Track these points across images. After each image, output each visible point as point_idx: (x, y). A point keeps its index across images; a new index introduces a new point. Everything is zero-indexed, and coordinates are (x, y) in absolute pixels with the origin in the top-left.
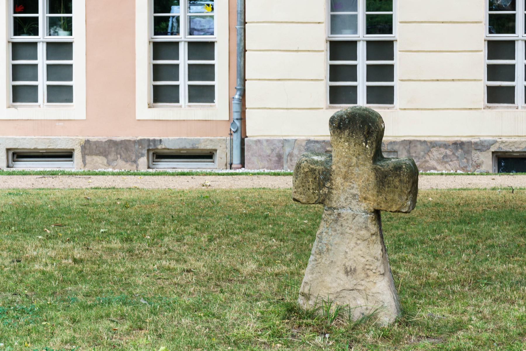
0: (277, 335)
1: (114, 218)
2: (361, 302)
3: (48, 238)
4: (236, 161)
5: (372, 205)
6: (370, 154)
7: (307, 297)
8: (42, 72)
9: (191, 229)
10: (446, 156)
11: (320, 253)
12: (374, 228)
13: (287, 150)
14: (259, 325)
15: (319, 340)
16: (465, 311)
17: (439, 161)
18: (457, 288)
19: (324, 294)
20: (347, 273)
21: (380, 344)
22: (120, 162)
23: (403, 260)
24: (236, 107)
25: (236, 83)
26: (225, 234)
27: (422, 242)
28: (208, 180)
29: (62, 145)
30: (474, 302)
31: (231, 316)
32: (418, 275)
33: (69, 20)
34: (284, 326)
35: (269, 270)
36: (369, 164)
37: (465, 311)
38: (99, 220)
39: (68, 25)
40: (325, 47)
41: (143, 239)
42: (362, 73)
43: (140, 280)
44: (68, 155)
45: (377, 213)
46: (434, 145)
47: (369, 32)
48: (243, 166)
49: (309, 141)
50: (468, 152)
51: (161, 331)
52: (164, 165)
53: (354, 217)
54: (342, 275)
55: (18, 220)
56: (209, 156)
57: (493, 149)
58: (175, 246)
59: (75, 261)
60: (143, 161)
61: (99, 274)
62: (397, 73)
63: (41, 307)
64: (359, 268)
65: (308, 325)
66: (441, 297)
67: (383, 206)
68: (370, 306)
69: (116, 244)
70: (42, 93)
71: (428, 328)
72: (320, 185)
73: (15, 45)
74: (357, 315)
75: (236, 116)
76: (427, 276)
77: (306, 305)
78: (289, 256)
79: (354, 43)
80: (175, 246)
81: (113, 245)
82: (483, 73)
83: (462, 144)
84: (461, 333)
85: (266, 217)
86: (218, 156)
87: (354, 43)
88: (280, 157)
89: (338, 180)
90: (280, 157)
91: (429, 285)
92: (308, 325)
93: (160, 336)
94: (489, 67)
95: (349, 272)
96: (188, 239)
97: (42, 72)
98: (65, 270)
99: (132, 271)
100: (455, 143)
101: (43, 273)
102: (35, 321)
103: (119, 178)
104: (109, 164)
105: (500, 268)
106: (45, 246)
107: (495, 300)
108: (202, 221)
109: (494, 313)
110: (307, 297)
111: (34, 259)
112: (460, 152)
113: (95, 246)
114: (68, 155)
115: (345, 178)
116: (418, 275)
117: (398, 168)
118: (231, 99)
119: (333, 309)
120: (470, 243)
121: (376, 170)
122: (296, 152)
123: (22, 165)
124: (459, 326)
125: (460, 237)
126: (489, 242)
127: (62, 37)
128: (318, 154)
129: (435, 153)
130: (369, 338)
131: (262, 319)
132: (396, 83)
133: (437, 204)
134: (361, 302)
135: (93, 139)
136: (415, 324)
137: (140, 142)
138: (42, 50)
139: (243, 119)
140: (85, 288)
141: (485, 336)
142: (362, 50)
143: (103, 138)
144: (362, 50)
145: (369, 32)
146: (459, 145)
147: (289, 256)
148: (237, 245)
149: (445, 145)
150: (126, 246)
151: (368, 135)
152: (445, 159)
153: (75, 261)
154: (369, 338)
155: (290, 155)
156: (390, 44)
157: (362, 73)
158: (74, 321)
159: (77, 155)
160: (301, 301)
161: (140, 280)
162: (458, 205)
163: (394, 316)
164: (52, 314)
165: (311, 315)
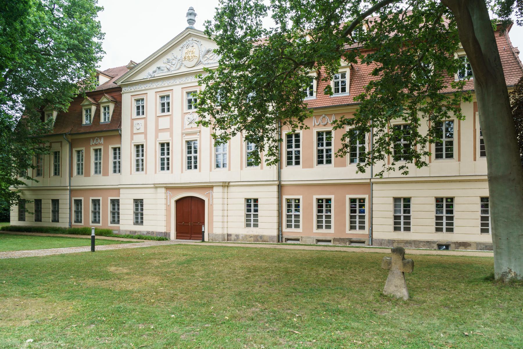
0: (378, 301)
1: (340, 262)
2: (399, 294)
3: (324, 267)
4: (370, 244)
5: (402, 271)
6: (401, 258)
7: (385, 291)
8: (324, 222)
9: (358, 266)
10: (424, 245)
11: (389, 281)
12: (402, 276)
13: (383, 242)
14: (373, 298)
15: (388, 303)
16: (426, 297)
17: (422, 246)
18: (425, 289)
19: (389, 291)
20: (395, 287)
21: (404, 305)
22: (342, 243)
23: (411, 279)
24: (370, 231)
25: (370, 225)
26: (366, 268)
27: (416, 273)
28: (363, 249)
29: (328, 239)
30: (429, 294)
31: (366, 294)
32: (415, 284)
33: (330, 210)
34: (379, 299)
35: (377, 281)
36: (401, 261)
37: (426, 297)
38: (336, 262)
39: (330, 211)
40: (393, 217)
41: (346, 269)
42: (402, 223)
43: (345, 282)
44: (330, 241)
45: (403, 273)
46: (421, 242)
47: (404, 213)
48: (372, 245)
49: (389, 240)
50: (430, 244)
51: (349, 298)
52: (353, 245)
53: (397, 273)
54: (394, 287)
55: (318, 261)
56: (364, 242)
57: (437, 243)
58: (354, 271)
59: (330, 275)
60: (348, 243)
61: (335, 279)
62: (454, 224)
63: (322, 289)
64: (399, 286)
65: (385, 299)
66: (420, 292)
67: (405, 271)
68: (401, 295)
69: (340, 270)
70: (324, 227)
71: (416, 302)
72: (389, 265)
73: (318, 216)
74: (398, 297)
75: (370, 233)
76: (417, 285)
77: (385, 294)
78: (382, 276)
79: (400, 216)
80: (354, 271)
81: (339, 271)
82: (434, 224)
83: (429, 242)
84: (425, 304)
85: (377, 263)
86: (366, 243)
87: (400, 216)
88: (381, 243)
89: (393, 264)
90: (381, 243)
91: (417, 288)
92: (385, 299)
93: (349, 300)
94: (436, 222)
95: (396, 286)
96: (357, 269)
97: (324, 222)
98: (328, 277)
99: (343, 279)
100: (427, 241)
101: (323, 278)
102: (320, 293)
103: (342, 248)
104: (339, 244)
105: (437, 283)
106: (323, 270)
107: (435, 294)
108: (361, 264)
109: (434, 298)
110: (385, 291)
111: (321, 274)
112: (428, 244)
113: (335, 271)
114: (330, 241)
115: (395, 264)
116: (415, 284)
117: (408, 262)
118: (369, 229)
119: (392, 295)
120: (429, 274)
121: (403, 262)
122: (385, 242)
123: (319, 243)
124: (424, 302)
125: (427, 272)
126: (434, 274)
127: (329, 214)
128: (388, 257)
129: (422, 244)
130: (401, 303)
131: (374, 296)
132: (411, 226)
133: (421, 261)
134: (399, 294)
135: (336, 238)
136: (413, 300)
137: (347, 239)
138: (324, 217)
139: (372, 234)
140: (332, 283)
141: (432, 305)
142: (402, 218)
143: (338, 237)
144: (402, 218)
145: (404, 213)
146: (428, 242)
147: (382, 276)
148: (369, 272)
149: (424, 242)
150: (342, 271)
151: (401, 254)
152: (424, 246)
153: (330, 275)
154: (401, 303)
155: (384, 243)
156: (410, 216)
157: (402, 223)
158: (329, 294)
159: (332, 241)
160: (384, 292)
161: (345, 282)
162: (427, 261)
163: (407, 298)
164: (324, 291)
165: (386, 296)
